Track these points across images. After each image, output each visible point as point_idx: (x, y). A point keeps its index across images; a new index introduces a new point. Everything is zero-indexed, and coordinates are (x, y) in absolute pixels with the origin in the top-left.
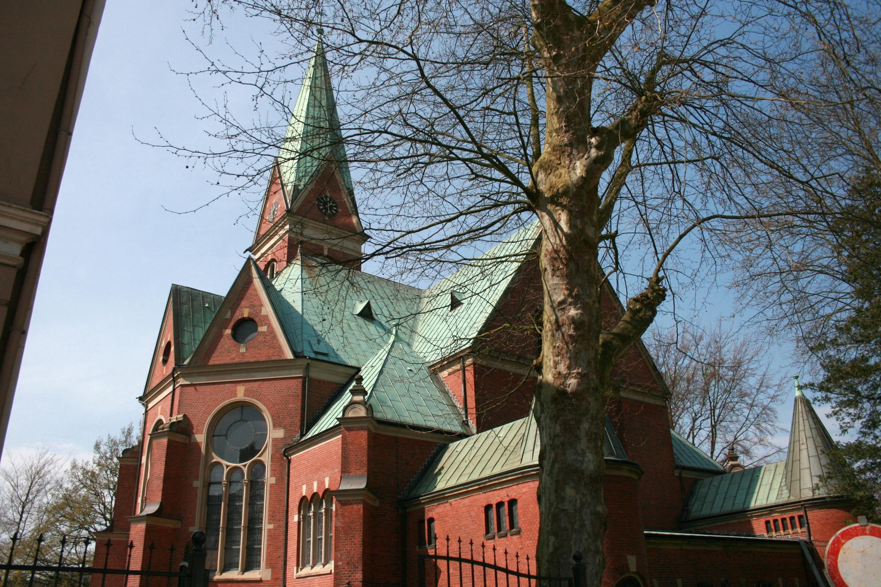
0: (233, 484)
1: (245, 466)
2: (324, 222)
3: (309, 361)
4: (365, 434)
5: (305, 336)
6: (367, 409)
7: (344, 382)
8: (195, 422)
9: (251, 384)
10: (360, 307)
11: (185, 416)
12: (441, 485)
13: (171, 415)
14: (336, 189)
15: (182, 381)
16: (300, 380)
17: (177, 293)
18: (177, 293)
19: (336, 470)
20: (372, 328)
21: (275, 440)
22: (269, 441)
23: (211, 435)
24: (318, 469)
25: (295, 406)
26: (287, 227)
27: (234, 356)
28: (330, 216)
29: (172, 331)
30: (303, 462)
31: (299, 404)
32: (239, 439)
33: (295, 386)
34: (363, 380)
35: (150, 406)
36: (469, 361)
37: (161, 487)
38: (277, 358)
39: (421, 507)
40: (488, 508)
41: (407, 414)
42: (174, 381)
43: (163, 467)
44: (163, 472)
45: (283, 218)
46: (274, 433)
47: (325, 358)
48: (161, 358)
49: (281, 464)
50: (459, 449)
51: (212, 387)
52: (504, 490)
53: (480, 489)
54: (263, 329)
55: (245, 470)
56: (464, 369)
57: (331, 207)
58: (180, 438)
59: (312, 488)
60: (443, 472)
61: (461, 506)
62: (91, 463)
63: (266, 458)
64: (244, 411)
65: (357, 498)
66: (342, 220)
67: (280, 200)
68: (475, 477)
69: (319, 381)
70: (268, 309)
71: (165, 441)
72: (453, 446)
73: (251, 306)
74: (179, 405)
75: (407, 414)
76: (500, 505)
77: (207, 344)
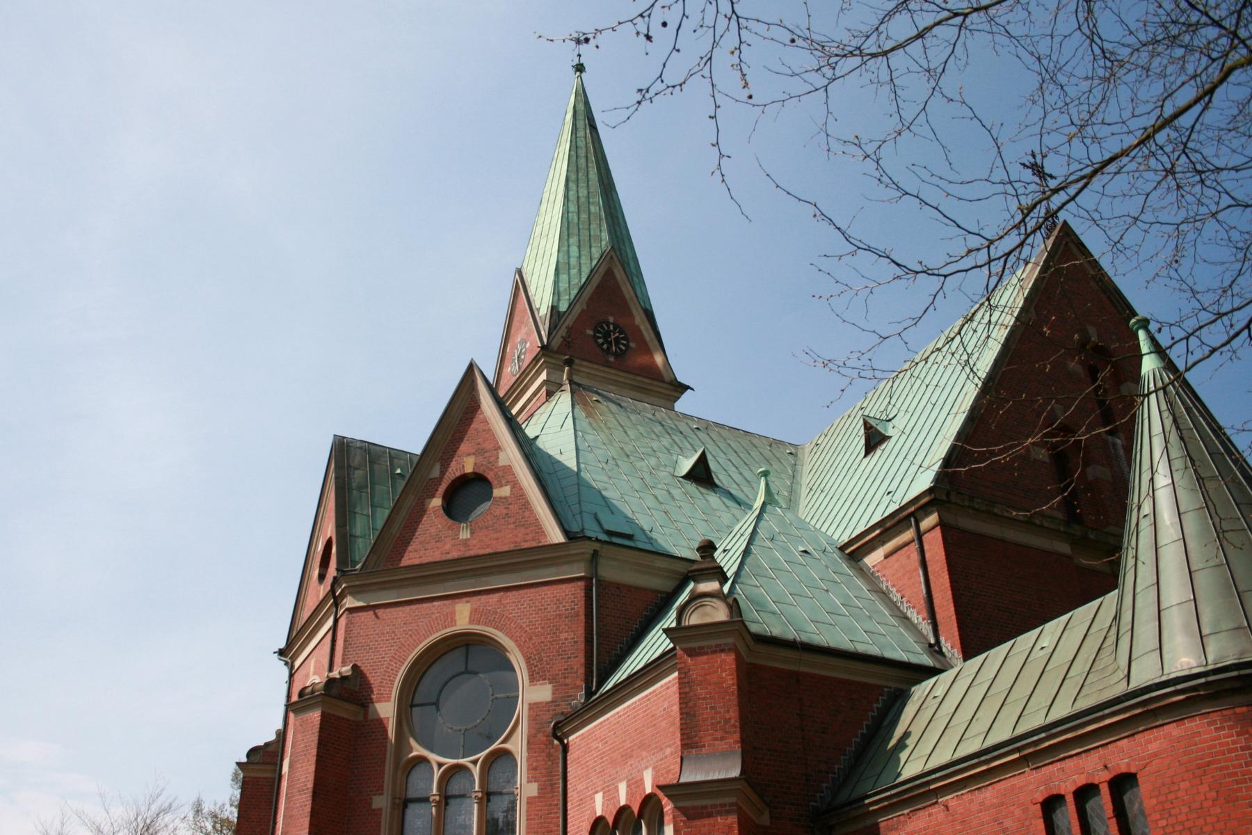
0: (452, 802)
1: (475, 762)
2: (608, 365)
3: (597, 546)
4: (729, 659)
5: (586, 507)
6: (730, 607)
7: (670, 590)
8: (374, 679)
9: (483, 598)
10: (686, 465)
11: (355, 668)
12: (911, 766)
13: (331, 669)
14: (623, 307)
15: (349, 602)
16: (581, 584)
17: (343, 450)
18: (343, 450)
19: (668, 751)
20: (714, 499)
21: (532, 707)
22: (522, 709)
23: (407, 703)
24: (627, 756)
25: (572, 635)
26: (543, 376)
27: (448, 547)
28: (616, 355)
29: (333, 520)
30: (594, 745)
31: (581, 631)
32: (463, 698)
33: (572, 596)
34: (716, 549)
35: (297, 664)
36: (926, 523)
37: (308, 809)
38: (534, 544)
39: (869, 822)
40: (1051, 805)
41: (812, 628)
42: (336, 604)
43: (312, 768)
44: (311, 777)
45: (536, 360)
46: (533, 694)
47: (624, 541)
48: (316, 572)
49: (549, 755)
50: (939, 692)
51: (407, 609)
52: (1094, 756)
53: (1024, 760)
54: (502, 492)
55: (476, 771)
56: (920, 536)
57: (617, 340)
58: (345, 711)
59: (617, 798)
60: (910, 742)
61: (974, 807)
62: (227, 806)
63: (518, 745)
64: (468, 652)
65: (719, 801)
66: (642, 360)
67: (528, 334)
68: (1002, 734)
69: (619, 586)
70: (510, 454)
71: (315, 716)
72: (920, 691)
73: (480, 452)
74: (345, 648)
75: (812, 628)
76: (1085, 793)
77: (396, 529)
